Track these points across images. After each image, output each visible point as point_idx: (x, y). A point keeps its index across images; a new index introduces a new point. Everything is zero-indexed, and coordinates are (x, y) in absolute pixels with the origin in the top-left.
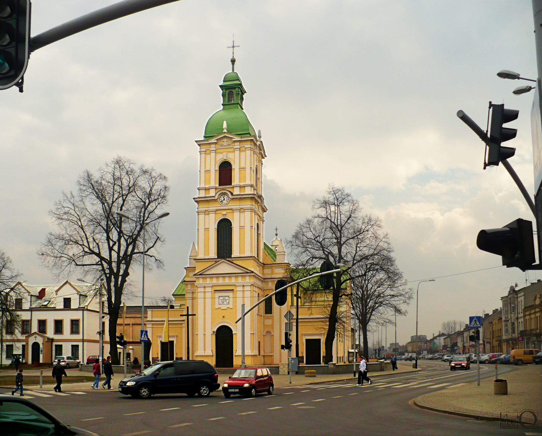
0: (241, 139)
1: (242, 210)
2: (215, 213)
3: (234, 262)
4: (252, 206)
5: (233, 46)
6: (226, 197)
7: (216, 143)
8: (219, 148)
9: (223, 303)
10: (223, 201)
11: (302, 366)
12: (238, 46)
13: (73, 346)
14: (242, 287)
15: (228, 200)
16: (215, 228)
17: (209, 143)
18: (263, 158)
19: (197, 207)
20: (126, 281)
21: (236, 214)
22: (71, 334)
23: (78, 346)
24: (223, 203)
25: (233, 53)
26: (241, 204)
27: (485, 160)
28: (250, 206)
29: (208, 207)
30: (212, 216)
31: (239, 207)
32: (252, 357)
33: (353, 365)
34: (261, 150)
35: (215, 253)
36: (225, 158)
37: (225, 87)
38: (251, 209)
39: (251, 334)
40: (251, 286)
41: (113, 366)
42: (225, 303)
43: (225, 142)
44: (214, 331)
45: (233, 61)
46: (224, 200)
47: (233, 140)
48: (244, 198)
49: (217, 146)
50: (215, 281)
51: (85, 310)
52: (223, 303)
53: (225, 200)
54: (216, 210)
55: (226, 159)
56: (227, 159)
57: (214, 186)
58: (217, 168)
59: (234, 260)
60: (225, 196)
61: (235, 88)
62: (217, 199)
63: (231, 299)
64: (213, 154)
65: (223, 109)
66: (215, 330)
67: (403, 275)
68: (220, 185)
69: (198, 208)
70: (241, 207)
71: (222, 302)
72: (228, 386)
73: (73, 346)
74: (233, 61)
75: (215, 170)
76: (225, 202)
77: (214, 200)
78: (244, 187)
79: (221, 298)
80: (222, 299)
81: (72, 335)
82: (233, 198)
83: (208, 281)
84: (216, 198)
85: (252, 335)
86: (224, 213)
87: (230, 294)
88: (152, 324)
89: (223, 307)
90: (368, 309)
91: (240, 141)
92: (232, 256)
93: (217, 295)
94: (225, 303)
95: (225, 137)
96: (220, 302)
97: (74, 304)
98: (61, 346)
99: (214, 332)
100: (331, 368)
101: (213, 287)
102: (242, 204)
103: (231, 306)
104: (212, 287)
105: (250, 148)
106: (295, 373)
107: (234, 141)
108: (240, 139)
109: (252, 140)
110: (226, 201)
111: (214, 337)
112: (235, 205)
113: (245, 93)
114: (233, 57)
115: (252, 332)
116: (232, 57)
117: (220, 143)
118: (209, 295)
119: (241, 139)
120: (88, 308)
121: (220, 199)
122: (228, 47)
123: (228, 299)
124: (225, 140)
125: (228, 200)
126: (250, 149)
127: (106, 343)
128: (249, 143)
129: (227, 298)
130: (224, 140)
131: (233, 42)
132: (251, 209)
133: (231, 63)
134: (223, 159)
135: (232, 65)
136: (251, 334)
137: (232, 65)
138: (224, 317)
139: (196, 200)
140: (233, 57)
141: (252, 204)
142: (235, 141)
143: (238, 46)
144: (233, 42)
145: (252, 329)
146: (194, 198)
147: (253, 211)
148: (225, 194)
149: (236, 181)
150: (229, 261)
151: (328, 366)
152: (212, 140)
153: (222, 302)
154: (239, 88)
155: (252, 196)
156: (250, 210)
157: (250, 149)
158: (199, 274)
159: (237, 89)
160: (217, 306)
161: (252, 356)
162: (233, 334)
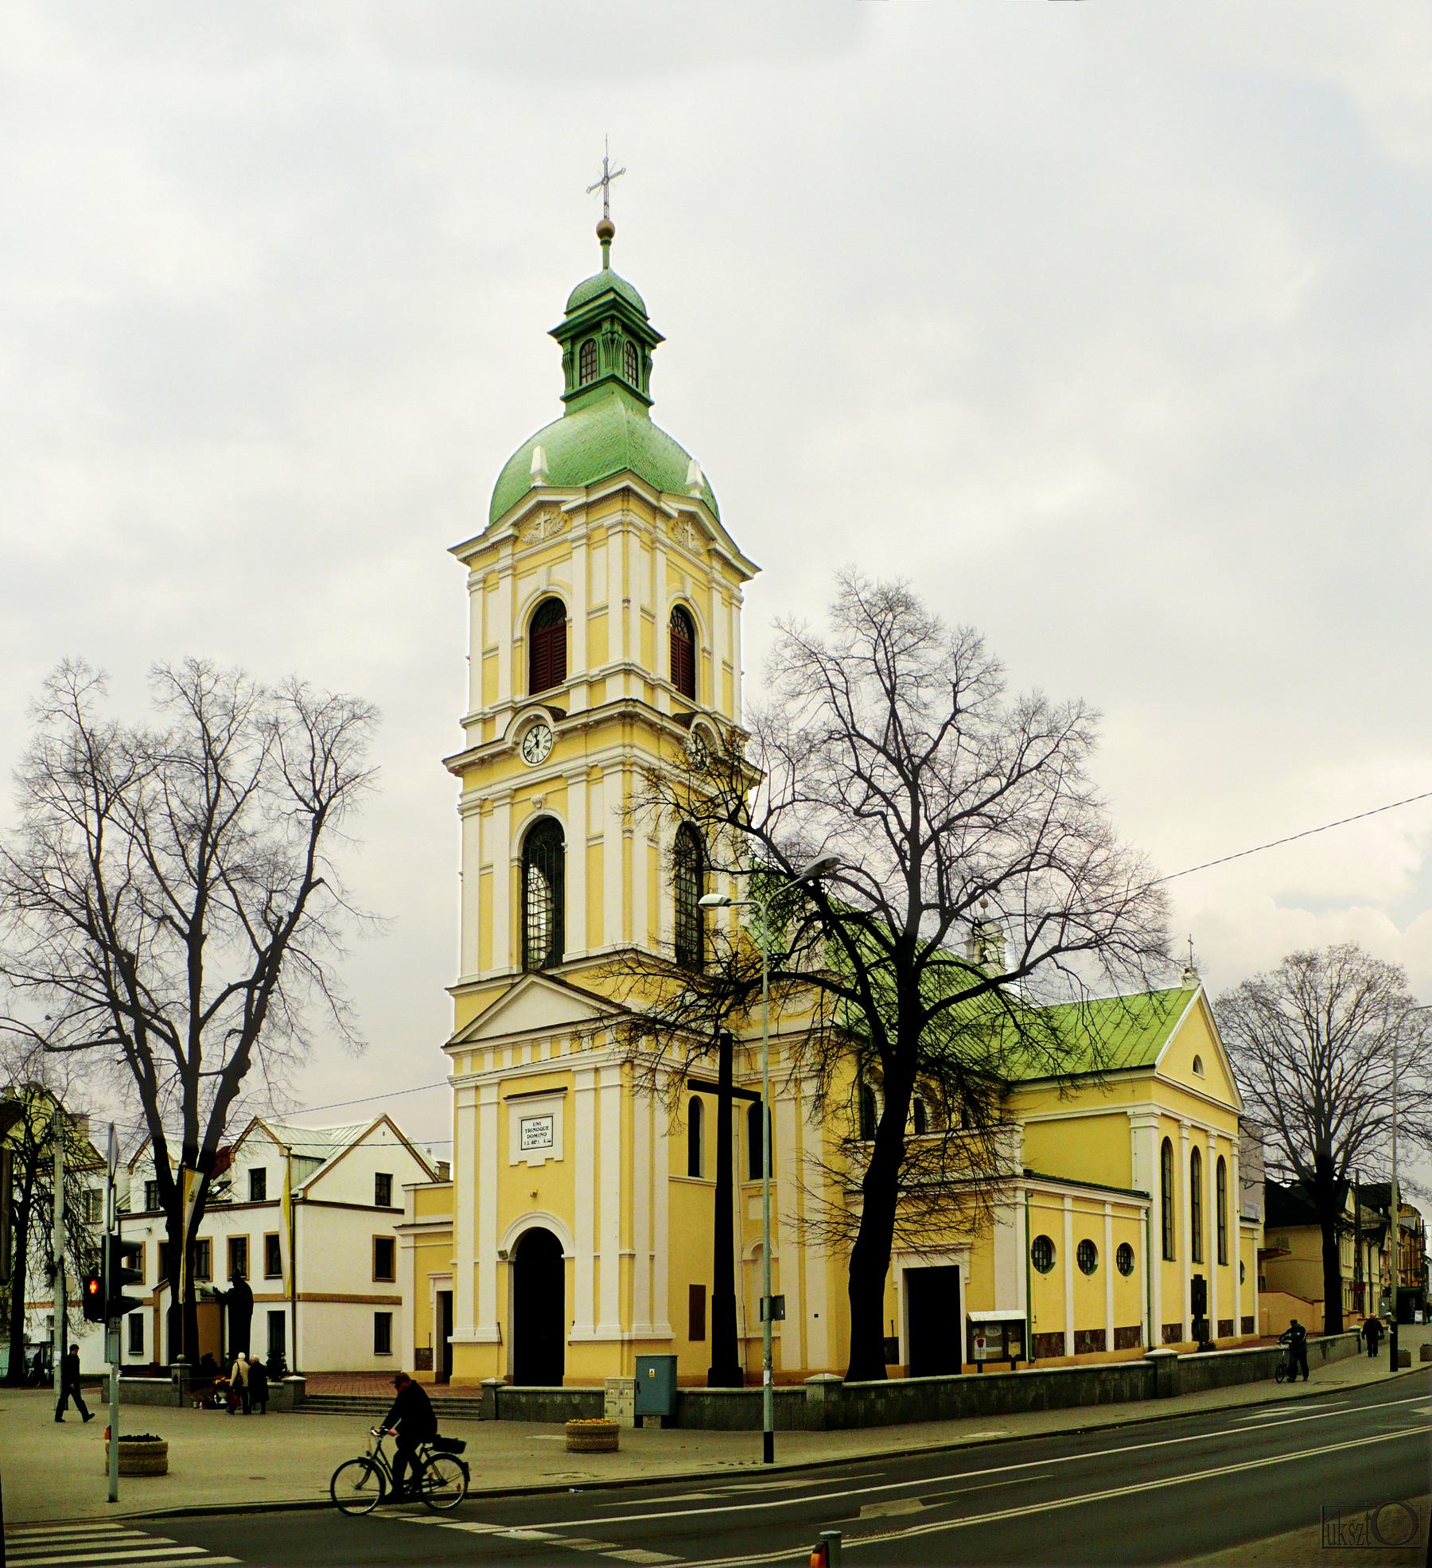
0: (588, 495)
1: (590, 775)
3: (569, 980)
4: (628, 749)
6: (543, 731)
7: (514, 539)
8: (523, 554)
9: (533, 1143)
10: (535, 750)
11: (691, 1393)
13: (377, 1315)
14: (591, 1075)
15: (548, 744)
16: (512, 861)
17: (493, 544)
18: (744, 577)
19: (461, 790)
20: (237, 1091)
21: (577, 792)
22: (267, 1278)
23: (283, 1313)
24: (529, 758)
26: (589, 752)
28: (620, 751)
29: (488, 783)
30: (502, 814)
31: (582, 761)
32: (626, 1347)
33: (761, 1394)
34: (713, 539)
35: (511, 955)
37: (566, 331)
38: (623, 764)
39: (621, 1256)
40: (621, 1065)
41: (272, 1387)
42: (541, 1141)
44: (502, 1249)
45: (606, 234)
46: (537, 744)
47: (564, 508)
48: (598, 723)
49: (520, 547)
50: (507, 1060)
51: (299, 1203)
52: (533, 1143)
53: (541, 745)
54: (516, 790)
55: (546, 592)
56: (551, 588)
58: (522, 631)
59: (576, 971)
60: (541, 728)
61: (597, 326)
62: (513, 749)
64: (506, 584)
65: (566, 415)
66: (508, 1246)
67: (1408, 985)
69: (461, 796)
70: (591, 760)
71: (530, 1140)
73: (377, 1315)
74: (606, 234)
75: (514, 642)
76: (540, 753)
78: (604, 679)
79: (528, 1125)
81: (269, 1281)
83: (488, 1063)
84: (510, 744)
85: (626, 1260)
86: (537, 794)
87: (554, 1106)
88: (416, 1236)
89: (536, 1157)
90: (1340, 1158)
91: (587, 507)
95: (541, 505)
96: (525, 1139)
97: (274, 1189)
98: (388, 1316)
99: (502, 1254)
100: (817, 1403)
101: (504, 1083)
102: (600, 748)
103: (556, 1152)
104: (499, 1084)
105: (621, 523)
106: (659, 1420)
107: (567, 512)
108: (582, 500)
109: (626, 492)
110: (545, 747)
111: (506, 1273)
112: (572, 756)
113: (657, 342)
115: (627, 1251)
116: (602, 218)
117: (529, 533)
118: (489, 1115)
119: (588, 495)
120: (310, 1197)
124: (542, 518)
125: (548, 744)
126: (620, 528)
127: (74, 1304)
128: (617, 504)
129: (546, 1122)
131: (606, 162)
132: (623, 764)
133: (599, 240)
134: (539, 593)
136: (621, 1256)
138: (535, 1195)
139: (453, 765)
141: (627, 742)
142: (572, 512)
143: (619, 173)
144: (606, 162)
145: (626, 1237)
146: (444, 761)
147: (635, 768)
148: (537, 721)
149: (577, 664)
150: (552, 978)
151: (804, 1393)
152: (503, 529)
153: (530, 1140)
154: (613, 317)
155: (622, 709)
156: (620, 767)
157: (620, 528)
158: (459, 1040)
159: (606, 326)
161: (622, 1342)
162: (563, 1261)
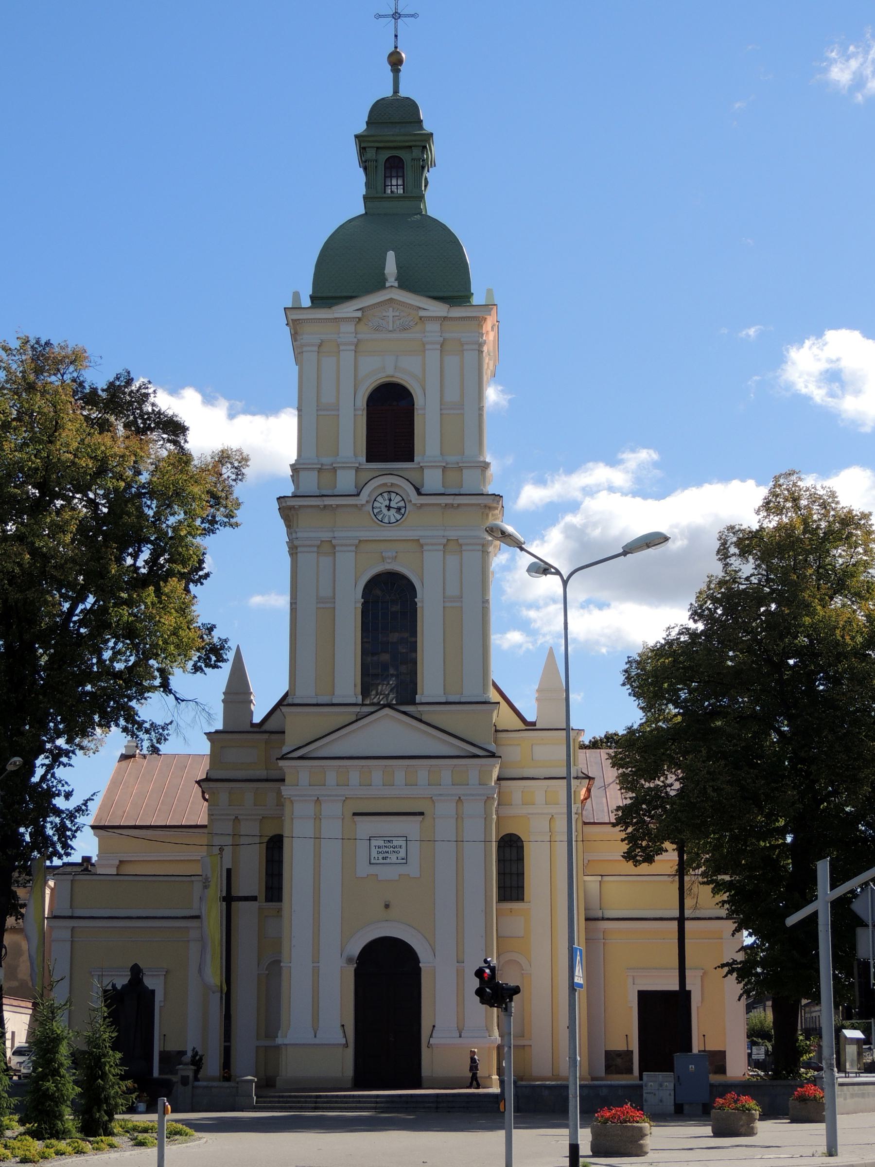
2: (318, 553)
5: (400, 16)
12: (412, 16)
25: (396, 36)
27: (326, 465)
36: (390, 371)
42: (393, 858)
43: (391, 318)
47: (422, 313)
53: (385, 510)
55: (392, 377)
57: (316, 461)
58: (362, 402)
62: (362, 505)
63: (414, 847)
66: (356, 949)
68: (369, 460)
72: (797, 1089)
77: (356, 506)
80: (381, 843)
82: (422, 505)
84: (364, 502)
92: (418, 698)
93: (367, 825)
94: (393, 858)
96: (374, 854)
114: (396, 47)
118: (332, 828)
121: (376, 504)
122: (379, 16)
123: (403, 844)
124: (390, 313)
130: (385, 314)
135: (391, 75)
137: (391, 74)
140: (396, 47)
150: (405, 713)
153: (381, 856)
160: (363, 869)
